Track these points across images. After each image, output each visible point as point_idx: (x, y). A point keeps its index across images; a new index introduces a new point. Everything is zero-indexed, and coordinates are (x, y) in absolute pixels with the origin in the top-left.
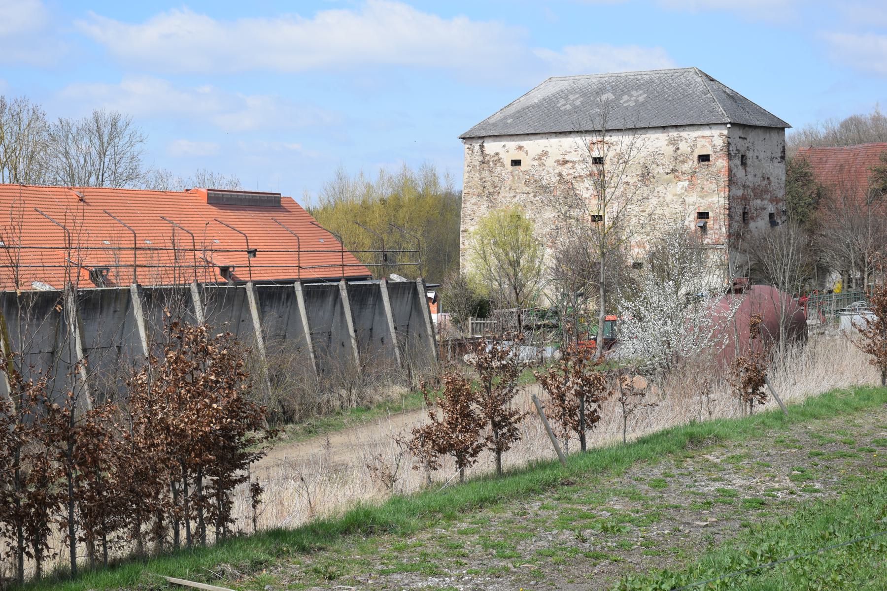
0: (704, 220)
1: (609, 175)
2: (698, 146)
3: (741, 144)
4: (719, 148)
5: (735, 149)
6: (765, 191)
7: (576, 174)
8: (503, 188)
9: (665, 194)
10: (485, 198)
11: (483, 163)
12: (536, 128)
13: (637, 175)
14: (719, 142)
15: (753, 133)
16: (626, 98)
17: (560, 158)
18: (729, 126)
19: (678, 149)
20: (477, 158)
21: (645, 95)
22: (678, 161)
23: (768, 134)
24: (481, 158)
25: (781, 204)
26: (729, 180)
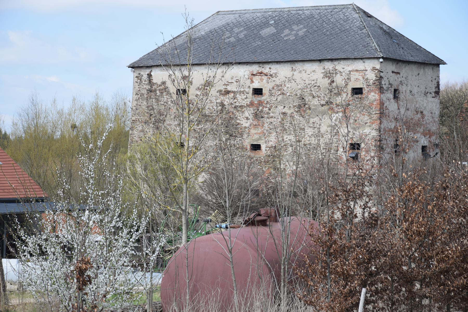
0: (356, 151)
1: (268, 106)
2: (352, 79)
3: (395, 80)
4: (371, 81)
5: (387, 83)
6: (418, 124)
7: (237, 104)
8: (168, 116)
9: (320, 125)
10: (151, 125)
11: (151, 91)
12: (201, 59)
13: (294, 106)
14: (372, 76)
15: (407, 68)
16: (287, 31)
17: (222, 88)
18: (381, 60)
19: (333, 82)
20: (145, 86)
21: (305, 30)
22: (332, 94)
23: (422, 70)
24: (148, 87)
25: (434, 137)
26: (380, 113)
